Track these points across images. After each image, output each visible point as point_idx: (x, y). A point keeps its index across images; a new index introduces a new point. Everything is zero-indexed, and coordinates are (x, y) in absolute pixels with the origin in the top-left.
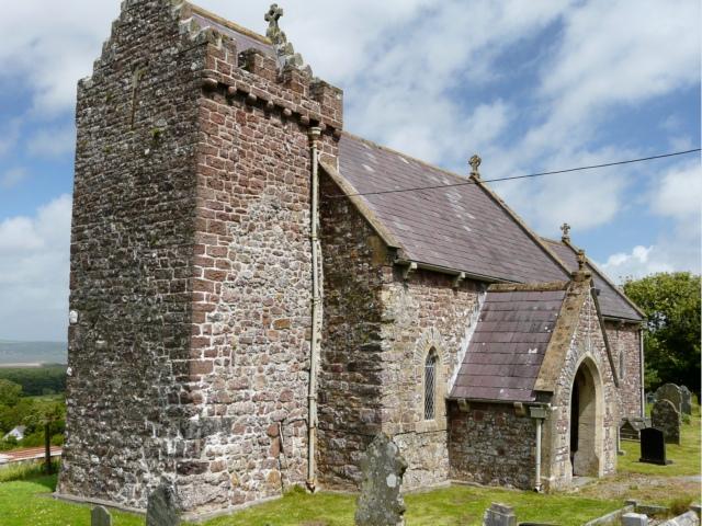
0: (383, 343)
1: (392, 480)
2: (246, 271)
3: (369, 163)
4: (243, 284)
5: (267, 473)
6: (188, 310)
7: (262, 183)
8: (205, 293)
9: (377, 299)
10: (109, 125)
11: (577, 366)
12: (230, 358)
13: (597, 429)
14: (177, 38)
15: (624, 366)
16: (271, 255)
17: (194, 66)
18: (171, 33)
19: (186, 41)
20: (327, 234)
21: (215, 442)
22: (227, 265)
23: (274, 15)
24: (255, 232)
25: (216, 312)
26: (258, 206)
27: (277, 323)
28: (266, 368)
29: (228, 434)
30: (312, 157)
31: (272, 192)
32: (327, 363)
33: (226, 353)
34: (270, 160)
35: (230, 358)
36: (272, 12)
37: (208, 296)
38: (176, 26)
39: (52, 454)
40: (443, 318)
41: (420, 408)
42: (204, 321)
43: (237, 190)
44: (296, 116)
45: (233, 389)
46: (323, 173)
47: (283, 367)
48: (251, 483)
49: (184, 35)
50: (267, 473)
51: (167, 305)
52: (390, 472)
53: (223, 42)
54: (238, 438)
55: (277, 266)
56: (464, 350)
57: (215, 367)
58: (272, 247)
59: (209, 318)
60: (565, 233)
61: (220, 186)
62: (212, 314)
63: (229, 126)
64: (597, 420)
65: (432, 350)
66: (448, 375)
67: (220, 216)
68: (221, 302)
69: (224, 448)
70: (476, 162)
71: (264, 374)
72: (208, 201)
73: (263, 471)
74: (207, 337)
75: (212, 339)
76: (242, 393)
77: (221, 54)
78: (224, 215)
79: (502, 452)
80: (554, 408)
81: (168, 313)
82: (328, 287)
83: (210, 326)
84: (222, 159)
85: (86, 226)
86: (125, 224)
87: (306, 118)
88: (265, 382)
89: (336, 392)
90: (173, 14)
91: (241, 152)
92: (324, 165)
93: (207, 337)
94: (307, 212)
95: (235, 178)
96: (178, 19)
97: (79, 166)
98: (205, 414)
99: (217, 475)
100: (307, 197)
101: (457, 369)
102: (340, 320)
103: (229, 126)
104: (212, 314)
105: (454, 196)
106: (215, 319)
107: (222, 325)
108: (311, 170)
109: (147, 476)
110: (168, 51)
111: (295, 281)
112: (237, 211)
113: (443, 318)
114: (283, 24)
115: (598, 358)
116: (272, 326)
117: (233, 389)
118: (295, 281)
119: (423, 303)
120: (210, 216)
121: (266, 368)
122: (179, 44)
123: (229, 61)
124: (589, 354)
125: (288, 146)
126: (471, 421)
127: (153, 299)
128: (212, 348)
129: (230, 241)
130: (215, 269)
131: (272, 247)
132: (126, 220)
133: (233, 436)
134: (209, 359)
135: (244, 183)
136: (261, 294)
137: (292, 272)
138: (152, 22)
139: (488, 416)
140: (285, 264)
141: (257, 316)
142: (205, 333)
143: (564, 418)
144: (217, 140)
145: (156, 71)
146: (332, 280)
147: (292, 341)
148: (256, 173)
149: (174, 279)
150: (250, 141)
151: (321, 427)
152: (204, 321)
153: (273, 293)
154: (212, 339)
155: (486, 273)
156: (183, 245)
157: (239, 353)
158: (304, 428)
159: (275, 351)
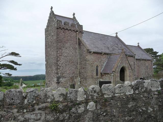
0: (87, 64)
2: (65, 54)
7: (68, 41)
11: (121, 67)
15: (148, 68)
22: (62, 54)
23: (74, 14)
26: (67, 45)
27: (72, 62)
28: (70, 69)
33: (63, 66)
34: (69, 38)
36: (73, 14)
41: (95, 74)
43: (63, 43)
44: (74, 30)
45: (64, 72)
46: (79, 39)
47: (73, 68)
48: (68, 85)
55: (71, 54)
58: (70, 51)
60: (138, 44)
61: (60, 43)
63: (62, 33)
65: (97, 66)
66: (101, 69)
75: (60, 65)
76: (66, 72)
87: (76, 31)
88: (70, 71)
91: (64, 37)
92: (79, 38)
95: (63, 41)
99: (61, 84)
101: (103, 68)
103: (62, 33)
106: (60, 62)
107: (62, 63)
114: (75, 16)
115: (126, 66)
117: (64, 72)
121: (70, 69)
124: (124, 65)
126: (104, 76)
128: (60, 66)
131: (70, 51)
136: (69, 58)
139: (106, 75)
141: (68, 61)
143: (118, 75)
147: (75, 65)
153: (71, 58)
154: (60, 65)
155: (109, 52)
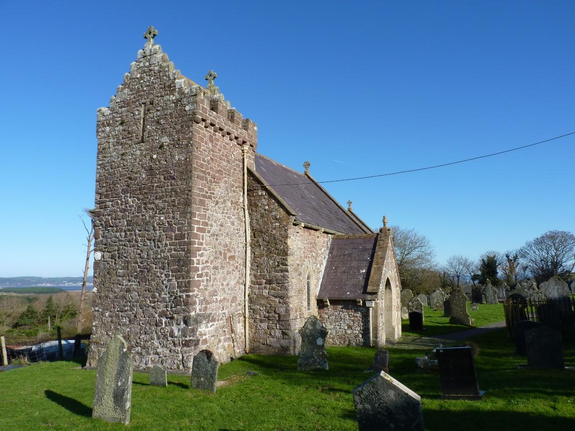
1: (319, 342)
3: (262, 166)
4: (214, 235)
5: (226, 344)
6: (188, 250)
8: (197, 240)
9: (286, 243)
10: (123, 138)
12: (208, 278)
13: (393, 312)
14: (174, 90)
16: (226, 218)
17: (187, 108)
18: (170, 86)
19: (181, 92)
20: (253, 206)
21: (202, 329)
24: (219, 205)
25: (202, 251)
28: (225, 283)
29: (208, 322)
30: (243, 162)
31: (226, 182)
32: (255, 280)
35: (208, 278)
37: (198, 242)
38: (173, 83)
39: (57, 341)
40: (313, 254)
42: (196, 257)
49: (179, 89)
50: (226, 344)
51: (173, 247)
52: (319, 337)
53: (204, 94)
54: (213, 325)
56: (323, 271)
57: (202, 283)
58: (227, 213)
59: (199, 255)
62: (200, 252)
64: (393, 308)
67: (204, 196)
68: (204, 246)
69: (207, 330)
70: (307, 165)
71: (224, 287)
72: (198, 186)
73: (225, 344)
74: (198, 266)
77: (203, 101)
78: (204, 195)
79: (350, 327)
80: (378, 301)
81: (173, 252)
82: (254, 235)
83: (199, 260)
84: (203, 162)
85: (108, 200)
86: (139, 199)
89: (260, 296)
90: (171, 76)
92: (249, 167)
93: (198, 266)
94: (242, 194)
96: (175, 79)
97: (100, 162)
98: (198, 311)
100: (242, 185)
102: (261, 256)
103: (206, 143)
104: (200, 252)
105: (303, 186)
106: (202, 255)
108: (243, 170)
109: (159, 350)
110: (168, 97)
111: (238, 233)
112: (210, 193)
113: (313, 254)
116: (227, 260)
118: (238, 233)
119: (305, 245)
120: (198, 195)
122: (176, 94)
123: (206, 106)
125: (233, 156)
127: (162, 244)
128: (200, 272)
129: (208, 210)
130: (201, 226)
132: (141, 197)
133: (211, 323)
134: (199, 279)
135: (214, 177)
137: (236, 229)
138: (154, 79)
140: (233, 224)
142: (197, 264)
144: (201, 151)
145: (159, 108)
146: (256, 233)
148: (218, 171)
149: (177, 232)
150: (216, 152)
151: (251, 317)
152: (196, 257)
154: (200, 266)
156: (184, 214)
157: (213, 274)
158: (242, 318)
159: (228, 273)
